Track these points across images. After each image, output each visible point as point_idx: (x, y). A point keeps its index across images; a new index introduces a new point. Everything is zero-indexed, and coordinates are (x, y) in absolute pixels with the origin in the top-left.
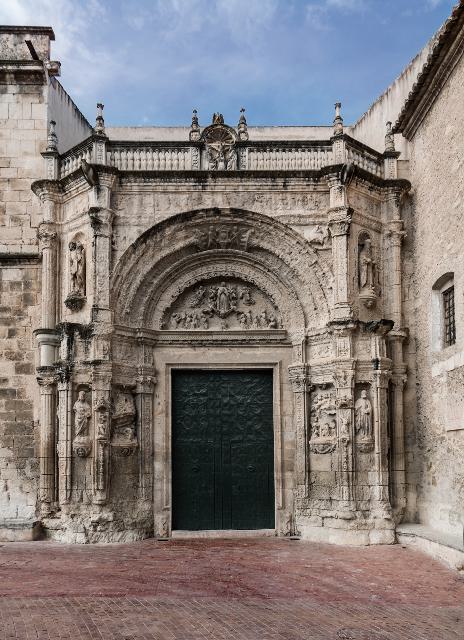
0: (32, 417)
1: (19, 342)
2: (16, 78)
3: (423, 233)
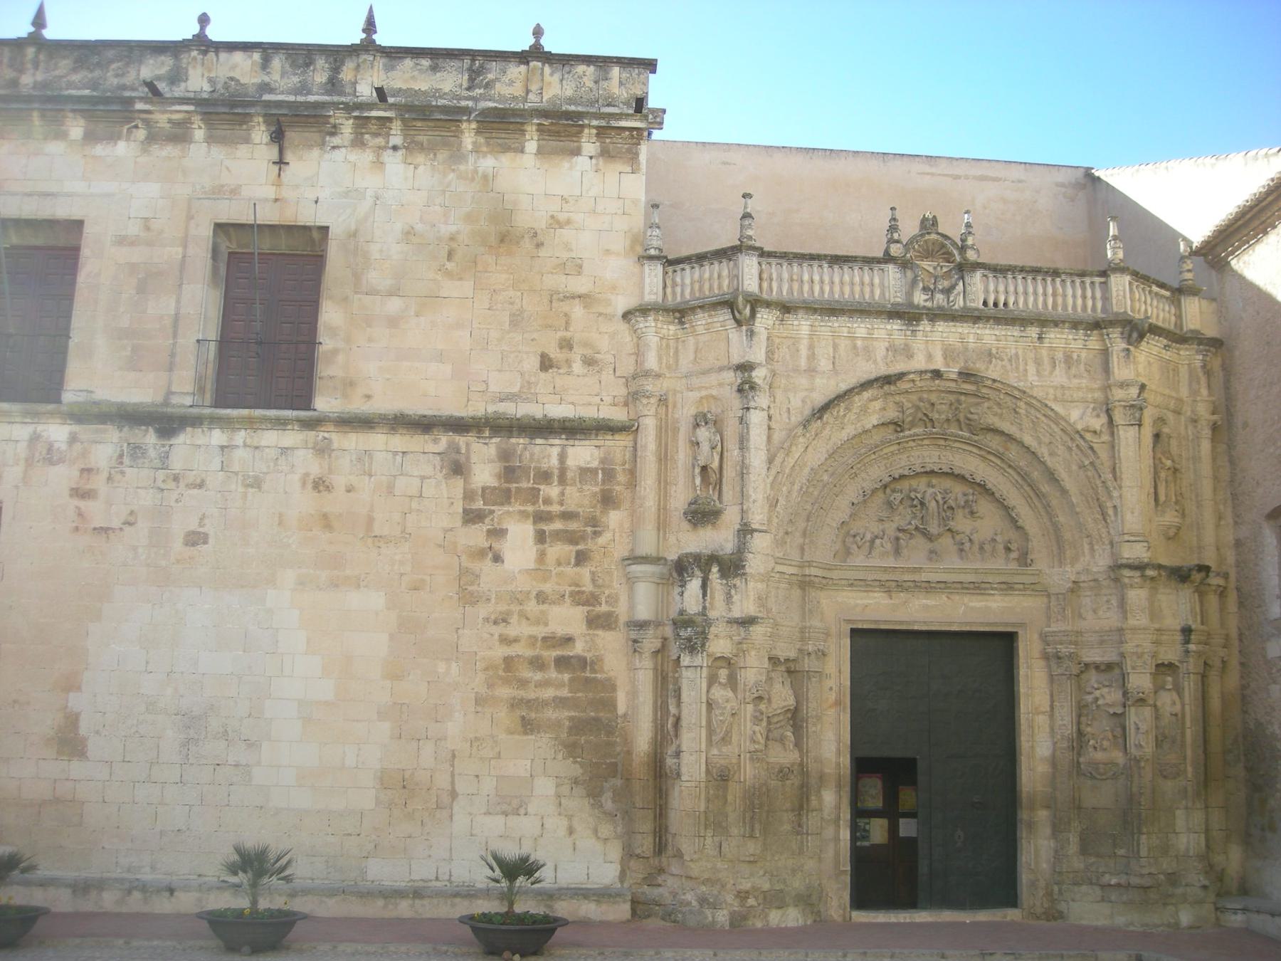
0: (615, 707)
1: (593, 573)
2: (598, 135)
3: (1245, 425)
